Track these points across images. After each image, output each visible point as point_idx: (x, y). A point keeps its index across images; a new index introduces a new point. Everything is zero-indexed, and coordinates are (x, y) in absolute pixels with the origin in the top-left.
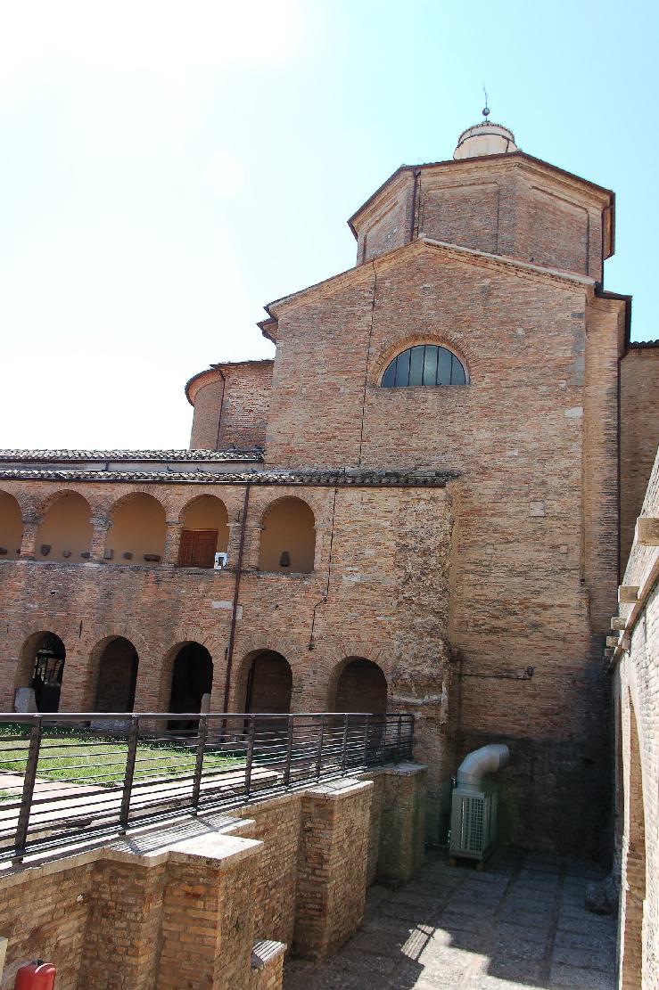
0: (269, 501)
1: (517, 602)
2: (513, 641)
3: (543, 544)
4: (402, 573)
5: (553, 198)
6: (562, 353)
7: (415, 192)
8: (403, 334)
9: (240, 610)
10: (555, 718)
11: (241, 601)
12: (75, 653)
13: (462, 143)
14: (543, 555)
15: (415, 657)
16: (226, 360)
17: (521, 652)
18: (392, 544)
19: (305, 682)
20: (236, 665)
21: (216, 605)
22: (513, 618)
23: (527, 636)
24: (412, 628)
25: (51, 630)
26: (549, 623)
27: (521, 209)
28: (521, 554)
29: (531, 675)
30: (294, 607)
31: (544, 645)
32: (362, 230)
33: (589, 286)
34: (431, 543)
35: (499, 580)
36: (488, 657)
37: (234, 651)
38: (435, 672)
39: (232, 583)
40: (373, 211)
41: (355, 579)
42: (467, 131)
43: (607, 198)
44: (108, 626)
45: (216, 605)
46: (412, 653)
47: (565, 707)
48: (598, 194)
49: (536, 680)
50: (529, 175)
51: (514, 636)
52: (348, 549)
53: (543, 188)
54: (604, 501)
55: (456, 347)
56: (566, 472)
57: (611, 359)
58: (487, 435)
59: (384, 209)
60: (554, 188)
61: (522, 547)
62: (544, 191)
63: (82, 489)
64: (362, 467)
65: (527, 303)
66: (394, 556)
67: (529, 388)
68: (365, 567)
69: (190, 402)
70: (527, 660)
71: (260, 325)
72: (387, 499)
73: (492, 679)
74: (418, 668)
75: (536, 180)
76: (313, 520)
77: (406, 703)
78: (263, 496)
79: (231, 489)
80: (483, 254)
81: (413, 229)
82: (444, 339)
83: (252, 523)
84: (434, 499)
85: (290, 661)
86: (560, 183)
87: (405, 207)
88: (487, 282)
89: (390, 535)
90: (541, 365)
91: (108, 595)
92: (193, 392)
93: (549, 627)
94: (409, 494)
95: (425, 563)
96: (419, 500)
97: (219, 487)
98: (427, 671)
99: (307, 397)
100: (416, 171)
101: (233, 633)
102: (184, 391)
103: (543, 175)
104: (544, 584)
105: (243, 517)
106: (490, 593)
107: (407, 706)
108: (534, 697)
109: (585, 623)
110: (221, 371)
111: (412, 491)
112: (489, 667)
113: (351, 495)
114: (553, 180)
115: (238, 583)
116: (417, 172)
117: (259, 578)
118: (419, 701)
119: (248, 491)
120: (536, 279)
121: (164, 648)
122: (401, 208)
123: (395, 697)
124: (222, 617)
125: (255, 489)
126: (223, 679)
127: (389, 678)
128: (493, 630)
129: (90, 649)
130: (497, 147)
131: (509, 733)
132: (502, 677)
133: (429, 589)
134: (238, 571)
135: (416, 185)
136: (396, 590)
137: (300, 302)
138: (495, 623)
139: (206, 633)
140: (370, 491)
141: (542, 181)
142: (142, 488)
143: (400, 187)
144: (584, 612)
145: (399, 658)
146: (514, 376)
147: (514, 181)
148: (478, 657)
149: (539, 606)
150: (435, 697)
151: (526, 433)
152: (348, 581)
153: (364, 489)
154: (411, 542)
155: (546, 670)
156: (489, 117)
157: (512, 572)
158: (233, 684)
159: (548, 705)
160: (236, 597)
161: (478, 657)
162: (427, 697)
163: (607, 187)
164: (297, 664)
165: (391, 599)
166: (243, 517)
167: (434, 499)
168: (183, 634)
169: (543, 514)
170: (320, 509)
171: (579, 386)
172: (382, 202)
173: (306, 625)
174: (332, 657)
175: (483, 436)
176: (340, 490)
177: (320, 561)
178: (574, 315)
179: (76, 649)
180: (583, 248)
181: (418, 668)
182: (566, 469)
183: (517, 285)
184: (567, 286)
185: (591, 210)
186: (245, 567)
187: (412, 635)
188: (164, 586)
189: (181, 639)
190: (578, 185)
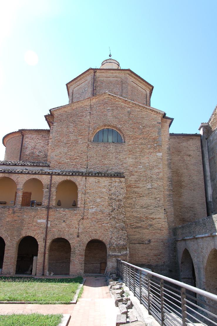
4: (111, 208)
5: (137, 86)
6: (155, 135)
7: (94, 77)
8: (101, 124)
9: (49, 222)
10: (159, 257)
11: (49, 219)
13: (104, 64)
15: (117, 238)
16: (24, 128)
17: (146, 234)
18: (107, 197)
19: (76, 250)
20: (48, 244)
21: (39, 221)
22: (142, 223)
23: (148, 229)
24: (116, 228)
28: (145, 201)
30: (71, 221)
31: (154, 232)
34: (120, 197)
36: (136, 237)
39: (46, 212)
40: (76, 82)
41: (94, 210)
42: (104, 61)
43: (151, 88)
45: (39, 221)
46: (116, 236)
47: (161, 253)
48: (149, 86)
49: (152, 244)
50: (131, 77)
51: (144, 229)
55: (120, 130)
56: (158, 174)
57: (168, 138)
59: (81, 82)
60: (137, 82)
61: (145, 198)
62: (135, 83)
64: (88, 170)
65: (143, 118)
66: (108, 202)
67: (145, 146)
68: (97, 206)
69: (4, 145)
70: (148, 237)
71: (46, 116)
72: (105, 181)
73: (137, 244)
74: (118, 242)
75: (133, 79)
77: (115, 255)
78: (57, 179)
80: (128, 100)
81: (94, 89)
82: (115, 127)
83: (53, 190)
84: (121, 182)
85: (70, 242)
86: (139, 81)
87: (90, 82)
88: (129, 109)
90: (148, 138)
92: (7, 139)
93: (155, 225)
94: (112, 180)
95: (119, 204)
96: (116, 182)
97: (39, 175)
100: (95, 70)
101: (46, 232)
102: (2, 138)
103: (135, 78)
104: (153, 211)
105: (50, 187)
106: (135, 214)
107: (116, 256)
108: (151, 250)
110: (22, 132)
111: (113, 179)
113: (91, 180)
114: (137, 80)
115: (48, 212)
116: (95, 71)
117: (57, 210)
118: (119, 254)
119: (51, 177)
120: (145, 110)
121: (17, 240)
122: (89, 83)
123: (110, 253)
125: (54, 177)
126: (43, 250)
127: (108, 246)
128: (137, 227)
130: (115, 67)
131: (144, 263)
134: (48, 208)
135: (94, 75)
136: (109, 214)
137: (63, 110)
139: (35, 232)
141: (134, 80)
142: (6, 175)
143: (88, 75)
144: (166, 220)
145: (111, 239)
147: (126, 78)
148: (132, 237)
149: (152, 218)
150: (125, 252)
151: (144, 160)
153: (96, 177)
154: (114, 197)
155: (155, 240)
157: (142, 207)
158: (47, 252)
159: (156, 252)
160: (48, 218)
161: (132, 237)
162: (122, 252)
163: (152, 85)
164: (73, 243)
165: (107, 217)
166: (50, 187)
167: (121, 182)
169: (151, 187)
170: (80, 184)
172: (81, 79)
173: (76, 228)
174: (86, 240)
175: (130, 161)
176: (88, 178)
177: (80, 204)
178: (158, 123)
181: (118, 242)
182: (158, 173)
183: (139, 111)
184: (155, 113)
185: (147, 91)
186: (51, 206)
187: (116, 230)
188: (16, 214)
189: (24, 235)
190: (144, 83)
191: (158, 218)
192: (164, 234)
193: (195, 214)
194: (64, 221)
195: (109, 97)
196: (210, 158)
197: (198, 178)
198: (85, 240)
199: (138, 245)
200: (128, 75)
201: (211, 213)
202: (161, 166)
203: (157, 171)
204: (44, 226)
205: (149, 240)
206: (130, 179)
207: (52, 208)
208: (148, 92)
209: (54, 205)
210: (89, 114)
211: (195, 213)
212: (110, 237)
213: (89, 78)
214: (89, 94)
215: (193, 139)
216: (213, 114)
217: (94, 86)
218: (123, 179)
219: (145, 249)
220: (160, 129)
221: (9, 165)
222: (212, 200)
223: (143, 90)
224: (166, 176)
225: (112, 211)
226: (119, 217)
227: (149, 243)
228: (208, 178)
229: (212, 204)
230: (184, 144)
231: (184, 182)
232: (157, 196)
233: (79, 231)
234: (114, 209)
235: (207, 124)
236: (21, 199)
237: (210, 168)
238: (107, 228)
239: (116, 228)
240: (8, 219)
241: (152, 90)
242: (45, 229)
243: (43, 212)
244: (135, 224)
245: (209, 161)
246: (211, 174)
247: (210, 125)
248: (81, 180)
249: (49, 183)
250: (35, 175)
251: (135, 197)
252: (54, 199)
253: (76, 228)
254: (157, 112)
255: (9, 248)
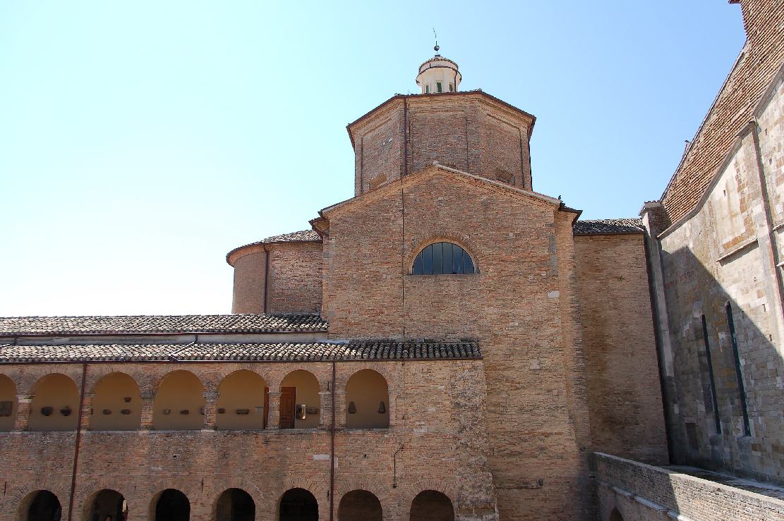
0: (351, 374)
1: (526, 432)
2: (526, 461)
3: (541, 389)
9: (336, 460)
11: (336, 453)
12: (199, 505)
14: (541, 397)
15: (473, 487)
17: (534, 469)
18: (447, 403)
21: (316, 457)
22: (525, 444)
23: (536, 457)
25: (175, 487)
26: (550, 446)
27: (482, 131)
29: (541, 485)
32: (359, 133)
33: (557, 205)
34: (477, 400)
35: (514, 417)
37: (334, 493)
38: (489, 497)
39: (328, 440)
41: (423, 431)
42: (423, 65)
44: (226, 480)
45: (316, 457)
46: (470, 484)
49: (546, 488)
50: (486, 107)
52: (415, 408)
53: (493, 115)
54: (574, 354)
58: (496, 311)
59: (378, 122)
60: (500, 115)
63: (194, 369)
72: (441, 370)
75: (489, 110)
76: (386, 386)
78: (346, 370)
79: (319, 365)
80: (481, 178)
83: (340, 391)
84: (474, 368)
85: (380, 498)
87: (398, 125)
88: (485, 197)
89: (445, 396)
90: (529, 260)
91: (225, 456)
98: (483, 498)
99: (359, 282)
105: (332, 386)
108: (545, 500)
109: (575, 444)
110: (266, 248)
111: (458, 362)
112: (511, 480)
119: (334, 366)
120: (519, 198)
121: (276, 497)
122: (395, 127)
124: (322, 467)
127: (455, 505)
128: (512, 454)
129: (212, 501)
132: (522, 488)
133: (478, 435)
134: (332, 430)
135: (406, 109)
136: (455, 438)
138: (512, 448)
140: (428, 363)
141: (492, 109)
144: (574, 437)
145: (462, 488)
146: (512, 268)
147: (476, 111)
149: (543, 434)
150: (491, 517)
151: (522, 310)
152: (419, 432)
154: (462, 401)
155: (552, 480)
156: (439, 52)
166: (332, 386)
167: (474, 368)
168: (291, 482)
171: (550, 281)
172: (377, 117)
173: (390, 469)
175: (491, 312)
176: (406, 363)
179: (200, 501)
180: (518, 156)
182: (552, 335)
185: (521, 128)
186: (337, 426)
190: (514, 113)
191: (556, 434)
192: (571, 467)
193: (636, 407)
194: (365, 456)
195: (441, 172)
196: (667, 283)
197: (641, 328)
198: (408, 493)
199: (516, 491)
200: (477, 103)
201: (671, 404)
202: (557, 320)
203: (550, 331)
204: (327, 466)
205: (539, 481)
206: (494, 351)
207: (339, 430)
208: (524, 130)
209: (343, 422)
210: (400, 213)
211: (637, 404)
212: (460, 485)
213: (395, 114)
214: (395, 173)
215: (626, 240)
216: (670, 185)
217: (405, 133)
218: (479, 363)
219: (532, 499)
220: (552, 238)
221: (249, 332)
222: (672, 375)
223: (510, 126)
224: (568, 337)
225: (460, 432)
226: (475, 443)
227: (539, 486)
228: (664, 327)
229: (674, 384)
230: (609, 253)
231: (611, 337)
232: (552, 387)
233: (397, 475)
234: (464, 428)
235: (658, 205)
236: (277, 413)
237: (667, 304)
238: (452, 467)
239: (469, 465)
240: (256, 457)
241: (533, 124)
242: (329, 474)
243: (325, 441)
244: (508, 446)
245: (665, 287)
246: (669, 317)
247: (665, 207)
248: (395, 369)
249: (330, 378)
250: (301, 364)
251: (506, 389)
252: (342, 410)
253: (390, 469)
254: (544, 201)
255: (263, 514)
